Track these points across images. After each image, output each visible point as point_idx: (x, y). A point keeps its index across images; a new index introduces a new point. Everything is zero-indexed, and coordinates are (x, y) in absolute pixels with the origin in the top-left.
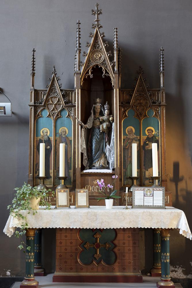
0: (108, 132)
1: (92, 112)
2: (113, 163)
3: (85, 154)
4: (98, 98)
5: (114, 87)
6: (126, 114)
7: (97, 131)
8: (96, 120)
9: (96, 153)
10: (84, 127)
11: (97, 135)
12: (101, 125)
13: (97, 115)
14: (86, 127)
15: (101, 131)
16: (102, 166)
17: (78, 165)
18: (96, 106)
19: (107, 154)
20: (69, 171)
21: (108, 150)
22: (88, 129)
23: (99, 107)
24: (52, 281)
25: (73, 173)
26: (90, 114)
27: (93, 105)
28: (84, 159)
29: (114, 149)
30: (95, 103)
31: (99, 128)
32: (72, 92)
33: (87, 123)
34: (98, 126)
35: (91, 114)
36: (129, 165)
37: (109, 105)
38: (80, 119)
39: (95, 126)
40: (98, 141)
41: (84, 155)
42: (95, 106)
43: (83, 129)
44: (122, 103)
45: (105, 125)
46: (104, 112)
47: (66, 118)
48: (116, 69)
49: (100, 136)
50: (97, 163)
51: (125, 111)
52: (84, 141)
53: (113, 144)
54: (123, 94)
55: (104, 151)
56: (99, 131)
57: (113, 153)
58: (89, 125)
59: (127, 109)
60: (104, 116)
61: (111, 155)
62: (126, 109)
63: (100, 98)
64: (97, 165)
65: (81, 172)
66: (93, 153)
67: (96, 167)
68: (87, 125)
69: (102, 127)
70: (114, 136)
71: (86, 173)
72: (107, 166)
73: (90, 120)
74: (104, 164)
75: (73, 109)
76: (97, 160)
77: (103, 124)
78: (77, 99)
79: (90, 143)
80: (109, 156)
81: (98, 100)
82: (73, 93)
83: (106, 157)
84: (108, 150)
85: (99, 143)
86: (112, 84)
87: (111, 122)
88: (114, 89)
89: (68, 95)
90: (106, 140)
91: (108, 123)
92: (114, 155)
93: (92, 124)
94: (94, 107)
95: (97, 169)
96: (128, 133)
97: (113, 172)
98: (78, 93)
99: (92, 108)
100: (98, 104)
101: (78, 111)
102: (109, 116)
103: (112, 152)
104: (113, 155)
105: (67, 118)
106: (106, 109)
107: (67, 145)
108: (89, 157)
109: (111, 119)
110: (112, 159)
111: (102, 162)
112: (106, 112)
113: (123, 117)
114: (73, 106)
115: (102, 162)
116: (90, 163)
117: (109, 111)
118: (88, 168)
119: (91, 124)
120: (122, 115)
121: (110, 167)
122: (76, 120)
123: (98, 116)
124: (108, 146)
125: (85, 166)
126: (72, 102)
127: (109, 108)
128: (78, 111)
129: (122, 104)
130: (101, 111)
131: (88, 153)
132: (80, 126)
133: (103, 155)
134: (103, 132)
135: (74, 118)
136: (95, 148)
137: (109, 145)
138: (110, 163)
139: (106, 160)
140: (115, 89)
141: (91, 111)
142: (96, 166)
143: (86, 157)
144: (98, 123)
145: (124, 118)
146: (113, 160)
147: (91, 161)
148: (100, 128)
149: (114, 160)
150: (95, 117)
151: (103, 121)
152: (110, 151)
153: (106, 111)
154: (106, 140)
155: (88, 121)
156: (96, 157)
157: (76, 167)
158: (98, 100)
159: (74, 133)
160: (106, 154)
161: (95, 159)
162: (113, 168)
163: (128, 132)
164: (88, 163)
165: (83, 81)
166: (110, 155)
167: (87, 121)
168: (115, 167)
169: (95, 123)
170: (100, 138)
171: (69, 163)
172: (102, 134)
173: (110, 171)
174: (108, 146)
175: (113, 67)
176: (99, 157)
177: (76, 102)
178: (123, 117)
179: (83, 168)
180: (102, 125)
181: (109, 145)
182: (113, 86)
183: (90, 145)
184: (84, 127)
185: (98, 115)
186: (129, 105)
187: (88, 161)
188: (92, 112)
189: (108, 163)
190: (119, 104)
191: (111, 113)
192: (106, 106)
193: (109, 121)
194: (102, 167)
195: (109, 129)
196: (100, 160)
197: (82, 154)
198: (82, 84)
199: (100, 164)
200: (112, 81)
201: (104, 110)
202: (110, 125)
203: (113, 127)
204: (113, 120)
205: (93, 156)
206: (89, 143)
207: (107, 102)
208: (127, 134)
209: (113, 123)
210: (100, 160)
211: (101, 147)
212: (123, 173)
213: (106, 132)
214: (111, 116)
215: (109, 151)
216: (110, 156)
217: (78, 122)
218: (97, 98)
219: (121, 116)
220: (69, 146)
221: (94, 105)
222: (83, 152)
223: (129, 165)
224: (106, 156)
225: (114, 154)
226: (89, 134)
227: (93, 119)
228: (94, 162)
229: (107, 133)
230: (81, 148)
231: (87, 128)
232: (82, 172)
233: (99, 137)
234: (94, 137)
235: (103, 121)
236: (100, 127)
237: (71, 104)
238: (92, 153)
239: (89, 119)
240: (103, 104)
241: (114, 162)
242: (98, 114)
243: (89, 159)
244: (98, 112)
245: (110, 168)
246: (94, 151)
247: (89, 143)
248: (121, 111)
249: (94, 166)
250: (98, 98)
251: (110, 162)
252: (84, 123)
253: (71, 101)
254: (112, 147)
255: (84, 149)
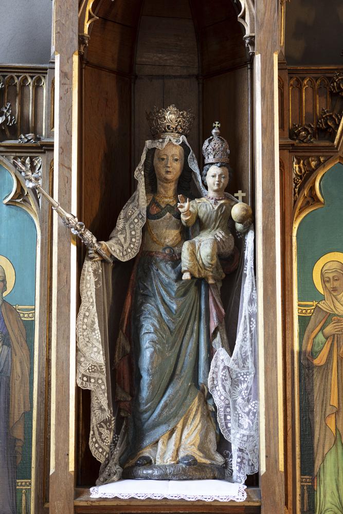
0: (223, 281)
1: (139, 175)
2: (248, 446)
3: (101, 399)
4: (172, 108)
5: (252, 43)
6: (313, 188)
7: (166, 273)
8: (158, 216)
9: (159, 392)
10: (96, 252)
11: (167, 298)
12: (186, 244)
13: (167, 193)
14: (103, 253)
15: (186, 276)
16: (189, 464)
17: (63, 459)
18: (157, 145)
19: (219, 398)
20: (16, 484)
21: (220, 374)
22: (116, 262)
23: (177, 151)
24: (91, 392)
25: (37, 498)
26: (132, 186)
27: (144, 145)
28: (94, 421)
29: (252, 370)
30: (156, 134)
31: (176, 260)
32: (39, 80)
33: (113, 233)
34: (171, 248)
35: (133, 185)
36: (333, 450)
37: (225, 144)
38: (74, 210)
39: (154, 248)
40: (172, 327)
41: (94, 402)
42: (154, 146)
43: (89, 266)
44: (293, 134)
45: (205, 245)
46: (204, 176)
47: (4, 206)
48: (91, 433)
49: (182, 299)
50: (166, 444)
51: (307, 176)
52: (96, 326)
53: (248, 343)
54: (299, 86)
55: (201, 380)
56: (173, 276)
57: (253, 394)
58: (123, 245)
59: (319, 165)
60: (199, 196)
61: (240, 400)
62: (313, 164)
63: (180, 108)
64: (164, 453)
65: (77, 495)
66: (145, 393)
67: (159, 467)
68: (112, 242)
69: (193, 254)
70: (252, 301)
71: (102, 503)
72: (219, 459)
73: (127, 219)
74: (202, 448)
75: (40, 161)
76: (163, 429)
77: (196, 239)
78: (60, 108)
79: (128, 335)
80: (228, 406)
81: (171, 116)
82: (45, 84)
83: (211, 415)
84: (220, 374)
85: (174, 336)
86: (243, 30)
87: (239, 226)
88: (253, 54)
89: (17, 95)
90: (214, 323)
91: (220, 234)
92: (252, 403)
93: (137, 241)
94: (152, 152)
95: (164, 477)
96: (325, 288)
97: (249, 499)
98: (65, 75)
99: (139, 160)
100: (168, 137)
101: (66, 93)
102: (226, 198)
103: (244, 386)
104: (248, 401)
105: (13, 210)
106: (210, 159)
107: (9, 345)
108: (122, 414)
109: (237, 210)
110: (246, 421)
111: (189, 438)
112: (214, 175)
113: (299, 204)
114: (42, 146)
115: (189, 438)
116: (128, 443)
117: (226, 169)
118: (117, 469)
119: (132, 236)
120: (298, 192)
121: (235, 468)
122: (55, 214)
123: (170, 201)
124: (221, 353)
125: (102, 460)
126: (35, 130)
127: (230, 156)
128: (66, 93)
129: (291, 137)
130: (186, 172)
131: (119, 390)
132: (74, 249)
133: (196, 400)
134: (198, 282)
135: (47, 207)
136: (152, 363)
137: (231, 351)
138: (234, 448)
139: (212, 426)
140: (258, 59)
141: (136, 173)
142: (159, 462)
143: (108, 414)
144: (171, 235)
145: (302, 210)
146: (250, 429)
147: (131, 432)
148: (180, 260)
149: (258, 430)
150: (153, 203)
151: (200, 224)
152: (235, 383)
153: (214, 170)
154: (214, 323)
155: (120, 224)
156: (160, 415)
157: (52, 471)
158: (171, 116)
159: (47, 286)
160: (210, 396)
161: (156, 425)
162: (247, 471)
163: (324, 281)
164: (114, 443)
165: (90, 17)
166: (235, 401)
167: (113, 225)
168: (263, 470)
169: (154, 232)
170: (180, 311)
171: (15, 439)
172: (193, 292)
173: (231, 491)
174: (221, 353)
175: (93, 428)
176: (177, 413)
177: (56, 130)
178: (299, 204)
179: (89, 471)
180: (193, 244)
181: (231, 351)
182: (252, 37)
183: (128, 349)
184: (96, 252)
185: (171, 193)
186: (327, 144)
187: (117, 431)
188: (139, 175)
189: (223, 445)
190: (280, 138)
191: (236, 181)
192: (212, 147)
193: (228, 223)
194: (192, 470)
195: (230, 264)
196: (180, 426)
197: (84, 397)
198: (86, 31)
199: (178, 451)
200: (243, 17)
201: (202, 165)
202: (232, 243)
203: (248, 254)
204: (250, 220)
205: (143, 408)
206: (122, 339)
207: (217, 124)
208: (321, 290)
209: (246, 233)
210: (180, 426)
211: (187, 359)
212: (302, 495)
213: (211, 281)
214: (240, 194)
215: (229, 382)
216: (235, 409)
217: (66, 223)
218: (165, 106)
219: (290, 199)
220: (20, 353)
221: (148, 143)
222: (90, 387)
223: (333, 450)
224: (212, 408)
225: (257, 397)
226: (126, 290)
227: (144, 213)
228: (147, 441)
229: (219, 285)
230: (78, 362)
231: (111, 256)
232: (83, 498)
233: (175, 307)
234: (149, 307)
235: (200, 224)
236: (180, 254)
237: (30, 136)
238: (139, 390)
239: (122, 214)
240: (196, 138)
241: (253, 438)
242: (171, 188)
243: (119, 421)
244: (169, 176)
245: (235, 473)
246: (146, 379)
247: (122, 339)
248: (291, 176)
249: (148, 462)
250: (172, 108)
251: (236, 440)
252: (94, 233)
253: (31, 124)
254: (244, 360)
255: (95, 368)
